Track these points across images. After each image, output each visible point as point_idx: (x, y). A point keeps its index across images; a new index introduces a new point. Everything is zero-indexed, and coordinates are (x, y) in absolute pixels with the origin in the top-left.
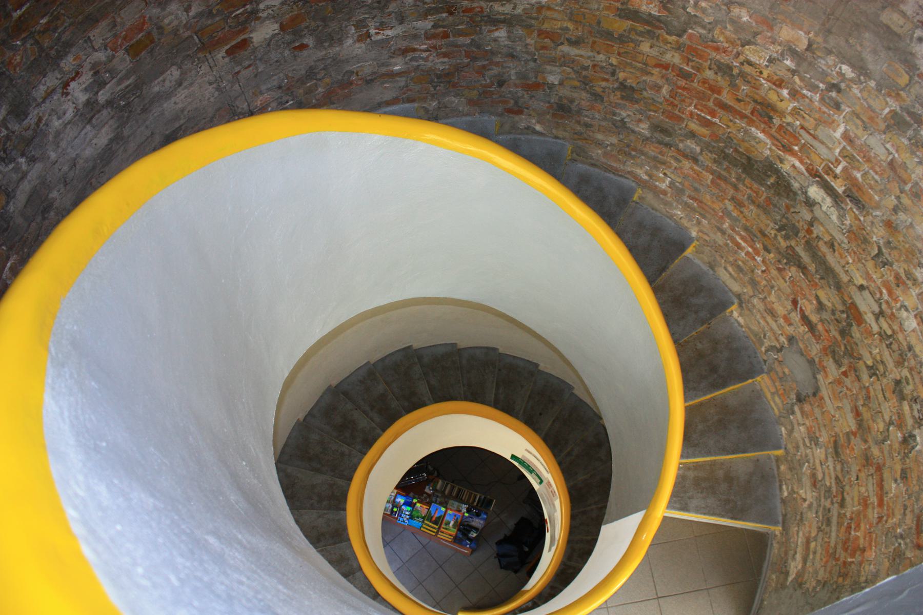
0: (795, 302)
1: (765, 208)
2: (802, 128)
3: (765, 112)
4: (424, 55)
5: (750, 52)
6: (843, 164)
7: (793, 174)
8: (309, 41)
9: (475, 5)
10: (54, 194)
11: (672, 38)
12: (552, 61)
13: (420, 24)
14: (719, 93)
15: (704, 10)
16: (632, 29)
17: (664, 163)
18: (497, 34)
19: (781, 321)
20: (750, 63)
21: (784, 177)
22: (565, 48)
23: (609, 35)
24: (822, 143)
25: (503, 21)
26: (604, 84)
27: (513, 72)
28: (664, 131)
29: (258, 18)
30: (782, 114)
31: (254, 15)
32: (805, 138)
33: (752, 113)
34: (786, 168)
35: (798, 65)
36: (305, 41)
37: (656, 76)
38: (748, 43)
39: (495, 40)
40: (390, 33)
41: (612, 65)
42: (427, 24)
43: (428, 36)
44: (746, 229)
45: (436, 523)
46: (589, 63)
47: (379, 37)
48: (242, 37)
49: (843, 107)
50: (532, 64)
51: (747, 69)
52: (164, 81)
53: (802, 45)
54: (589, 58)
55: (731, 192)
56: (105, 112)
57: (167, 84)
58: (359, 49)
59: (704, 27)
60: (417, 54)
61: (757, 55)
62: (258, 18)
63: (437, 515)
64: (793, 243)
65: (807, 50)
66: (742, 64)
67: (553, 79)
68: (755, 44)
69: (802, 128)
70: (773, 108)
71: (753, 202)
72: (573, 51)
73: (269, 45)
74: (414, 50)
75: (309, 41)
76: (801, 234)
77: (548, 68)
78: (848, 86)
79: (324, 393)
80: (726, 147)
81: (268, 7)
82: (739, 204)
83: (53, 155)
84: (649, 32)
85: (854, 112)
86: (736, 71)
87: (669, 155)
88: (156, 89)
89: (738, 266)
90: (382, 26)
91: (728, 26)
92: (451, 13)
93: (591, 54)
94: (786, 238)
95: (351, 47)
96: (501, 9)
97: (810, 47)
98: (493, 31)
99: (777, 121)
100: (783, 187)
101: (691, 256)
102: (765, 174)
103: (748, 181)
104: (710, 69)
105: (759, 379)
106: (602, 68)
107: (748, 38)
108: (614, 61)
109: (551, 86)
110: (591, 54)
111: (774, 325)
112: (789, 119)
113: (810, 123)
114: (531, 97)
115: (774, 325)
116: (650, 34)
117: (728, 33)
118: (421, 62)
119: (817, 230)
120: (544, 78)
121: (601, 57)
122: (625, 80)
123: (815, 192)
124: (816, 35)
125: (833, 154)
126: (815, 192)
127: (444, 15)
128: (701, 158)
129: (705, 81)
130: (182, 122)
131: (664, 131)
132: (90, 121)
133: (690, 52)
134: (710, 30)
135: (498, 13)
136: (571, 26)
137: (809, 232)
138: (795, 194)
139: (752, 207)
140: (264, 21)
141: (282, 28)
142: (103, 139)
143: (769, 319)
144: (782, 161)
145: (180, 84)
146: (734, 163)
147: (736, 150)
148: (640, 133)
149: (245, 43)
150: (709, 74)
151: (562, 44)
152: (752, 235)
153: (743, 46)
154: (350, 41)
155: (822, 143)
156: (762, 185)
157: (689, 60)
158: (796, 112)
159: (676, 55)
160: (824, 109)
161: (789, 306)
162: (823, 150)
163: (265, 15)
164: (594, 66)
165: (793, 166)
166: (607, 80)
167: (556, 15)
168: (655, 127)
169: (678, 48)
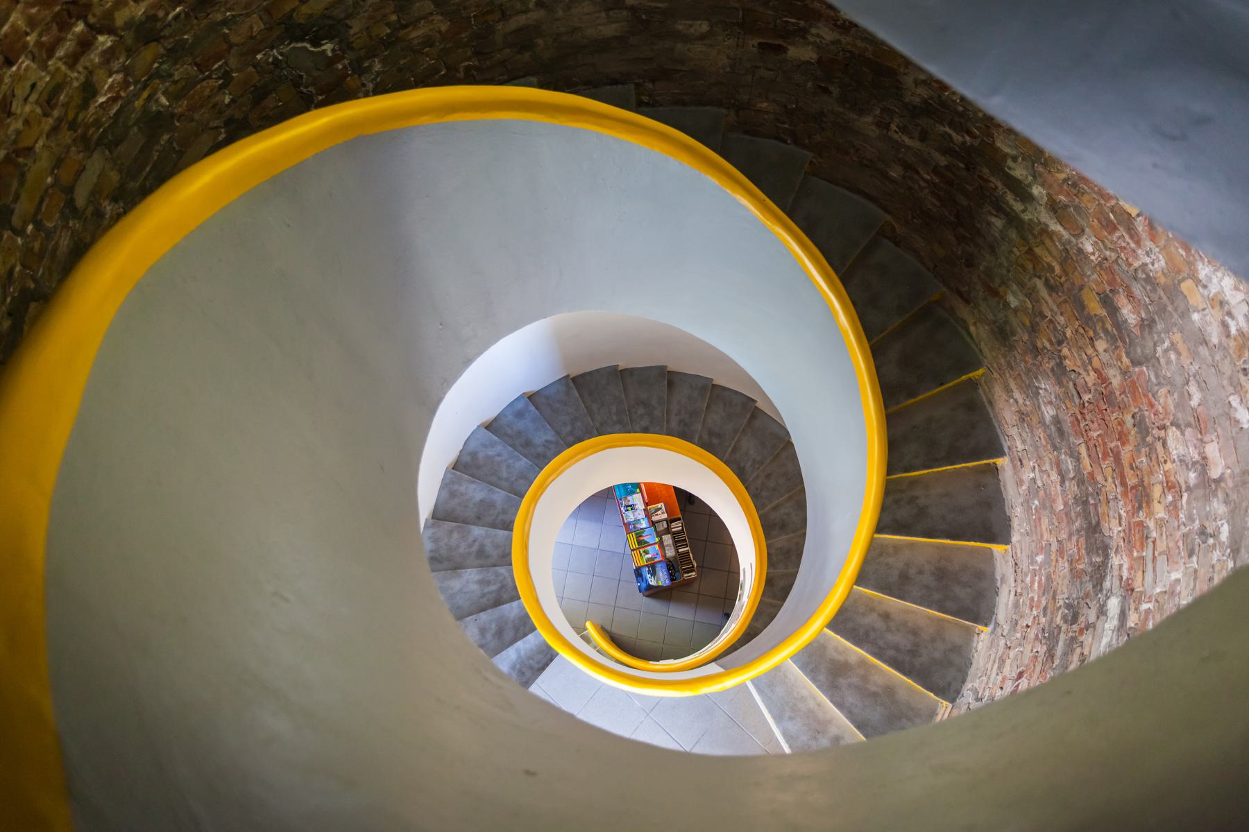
0: (1020, 675)
1: (1076, 575)
2: (1154, 542)
3: (1141, 497)
4: (923, 184)
5: (1172, 434)
6: (1150, 605)
7: (1116, 573)
8: (835, 90)
9: (993, 179)
10: (540, 41)
11: (1125, 360)
12: (1021, 285)
13: (936, 155)
14: (1123, 444)
15: (1169, 362)
16: (1102, 320)
17: (1040, 458)
18: (993, 219)
19: (1000, 678)
20: (1164, 444)
21: (1107, 567)
22: (1039, 284)
23: (1081, 306)
24: (1154, 571)
25: (1007, 215)
26: (1047, 345)
27: (985, 263)
28: (1061, 432)
29: (804, 38)
30: (1150, 514)
31: (803, 33)
32: (1147, 553)
33: (1132, 488)
34: (1115, 561)
35: (1196, 486)
36: (831, 88)
37: (1091, 378)
38: (1178, 427)
39: (989, 224)
40: (906, 140)
41: (1065, 334)
42: (943, 161)
43: (936, 170)
44: (1049, 578)
45: (640, 542)
46: (1049, 314)
47: (896, 137)
48: (780, 42)
49: (1194, 558)
50: (1004, 272)
51: (1159, 446)
52: (691, 26)
53: (1215, 473)
54: (1051, 310)
55: (1064, 536)
56: (625, 13)
57: (692, 30)
58: (873, 132)
59: (1157, 376)
60: (916, 177)
61: (1178, 444)
62: (804, 38)
63: (646, 539)
64: (1064, 628)
65: (1214, 480)
66: (1159, 439)
67: (1013, 301)
68: (1183, 434)
69: (1154, 542)
70: (1149, 502)
71: (1071, 562)
72: (1044, 292)
73: (799, 66)
74: (917, 172)
75: (835, 90)
76: (1075, 627)
77: (1015, 287)
78: (1214, 545)
79: (656, 367)
80: (1092, 495)
81: (818, 36)
82: (1061, 551)
83: (560, 13)
84: (1113, 337)
85: (1196, 571)
86: (1149, 439)
87: (1048, 457)
88: (680, 27)
89: (1017, 602)
90: (903, 129)
91: (1176, 396)
92: (968, 169)
93: (1055, 308)
94: (1064, 618)
95: (866, 123)
96: (1012, 202)
97: (1218, 481)
98: (992, 214)
99: (1142, 515)
100: (1099, 573)
101: (995, 554)
102: (1098, 549)
103: (1082, 540)
104: (1133, 417)
105: (945, 703)
106: (1055, 328)
107: (1181, 422)
108: (1069, 333)
109: (1007, 305)
110: (1055, 308)
111: (994, 675)
112: (1151, 524)
113: (1161, 546)
114: (985, 299)
115: (994, 675)
116: (1112, 340)
117: (1170, 401)
118: (916, 187)
119: (1087, 638)
120: (1006, 294)
121: (1062, 320)
122: (1065, 358)
123: (1114, 604)
124: (1233, 476)
125: (1154, 588)
126: (1114, 604)
127: (962, 165)
128: (1067, 484)
129: (1121, 423)
130: (684, 68)
131: (1061, 432)
132: (608, 10)
133: (1132, 387)
134: (1159, 384)
135: (1007, 203)
136: (1057, 269)
137: (1081, 631)
138: (1101, 590)
139: (1066, 565)
140: (809, 43)
141: (819, 61)
142: (609, 31)
143: (996, 666)
144: (1117, 552)
145: (702, 37)
146: (1085, 514)
147: (1095, 505)
148: (1042, 413)
149: (780, 49)
150: (1129, 419)
151: (1039, 277)
152: (1049, 589)
153: (1172, 424)
154: (869, 119)
155: (1154, 571)
156: (1088, 554)
157: (1124, 392)
158: (1160, 524)
159: (1119, 377)
160: (1180, 544)
161: (1014, 675)
162: (1149, 576)
163: (811, 39)
164: (1051, 321)
165: (1121, 566)
166: (1051, 343)
167: (1053, 249)
168: (1057, 421)
169: (1125, 373)
